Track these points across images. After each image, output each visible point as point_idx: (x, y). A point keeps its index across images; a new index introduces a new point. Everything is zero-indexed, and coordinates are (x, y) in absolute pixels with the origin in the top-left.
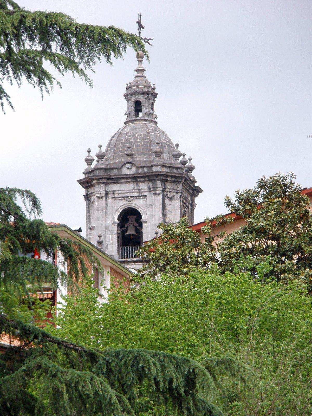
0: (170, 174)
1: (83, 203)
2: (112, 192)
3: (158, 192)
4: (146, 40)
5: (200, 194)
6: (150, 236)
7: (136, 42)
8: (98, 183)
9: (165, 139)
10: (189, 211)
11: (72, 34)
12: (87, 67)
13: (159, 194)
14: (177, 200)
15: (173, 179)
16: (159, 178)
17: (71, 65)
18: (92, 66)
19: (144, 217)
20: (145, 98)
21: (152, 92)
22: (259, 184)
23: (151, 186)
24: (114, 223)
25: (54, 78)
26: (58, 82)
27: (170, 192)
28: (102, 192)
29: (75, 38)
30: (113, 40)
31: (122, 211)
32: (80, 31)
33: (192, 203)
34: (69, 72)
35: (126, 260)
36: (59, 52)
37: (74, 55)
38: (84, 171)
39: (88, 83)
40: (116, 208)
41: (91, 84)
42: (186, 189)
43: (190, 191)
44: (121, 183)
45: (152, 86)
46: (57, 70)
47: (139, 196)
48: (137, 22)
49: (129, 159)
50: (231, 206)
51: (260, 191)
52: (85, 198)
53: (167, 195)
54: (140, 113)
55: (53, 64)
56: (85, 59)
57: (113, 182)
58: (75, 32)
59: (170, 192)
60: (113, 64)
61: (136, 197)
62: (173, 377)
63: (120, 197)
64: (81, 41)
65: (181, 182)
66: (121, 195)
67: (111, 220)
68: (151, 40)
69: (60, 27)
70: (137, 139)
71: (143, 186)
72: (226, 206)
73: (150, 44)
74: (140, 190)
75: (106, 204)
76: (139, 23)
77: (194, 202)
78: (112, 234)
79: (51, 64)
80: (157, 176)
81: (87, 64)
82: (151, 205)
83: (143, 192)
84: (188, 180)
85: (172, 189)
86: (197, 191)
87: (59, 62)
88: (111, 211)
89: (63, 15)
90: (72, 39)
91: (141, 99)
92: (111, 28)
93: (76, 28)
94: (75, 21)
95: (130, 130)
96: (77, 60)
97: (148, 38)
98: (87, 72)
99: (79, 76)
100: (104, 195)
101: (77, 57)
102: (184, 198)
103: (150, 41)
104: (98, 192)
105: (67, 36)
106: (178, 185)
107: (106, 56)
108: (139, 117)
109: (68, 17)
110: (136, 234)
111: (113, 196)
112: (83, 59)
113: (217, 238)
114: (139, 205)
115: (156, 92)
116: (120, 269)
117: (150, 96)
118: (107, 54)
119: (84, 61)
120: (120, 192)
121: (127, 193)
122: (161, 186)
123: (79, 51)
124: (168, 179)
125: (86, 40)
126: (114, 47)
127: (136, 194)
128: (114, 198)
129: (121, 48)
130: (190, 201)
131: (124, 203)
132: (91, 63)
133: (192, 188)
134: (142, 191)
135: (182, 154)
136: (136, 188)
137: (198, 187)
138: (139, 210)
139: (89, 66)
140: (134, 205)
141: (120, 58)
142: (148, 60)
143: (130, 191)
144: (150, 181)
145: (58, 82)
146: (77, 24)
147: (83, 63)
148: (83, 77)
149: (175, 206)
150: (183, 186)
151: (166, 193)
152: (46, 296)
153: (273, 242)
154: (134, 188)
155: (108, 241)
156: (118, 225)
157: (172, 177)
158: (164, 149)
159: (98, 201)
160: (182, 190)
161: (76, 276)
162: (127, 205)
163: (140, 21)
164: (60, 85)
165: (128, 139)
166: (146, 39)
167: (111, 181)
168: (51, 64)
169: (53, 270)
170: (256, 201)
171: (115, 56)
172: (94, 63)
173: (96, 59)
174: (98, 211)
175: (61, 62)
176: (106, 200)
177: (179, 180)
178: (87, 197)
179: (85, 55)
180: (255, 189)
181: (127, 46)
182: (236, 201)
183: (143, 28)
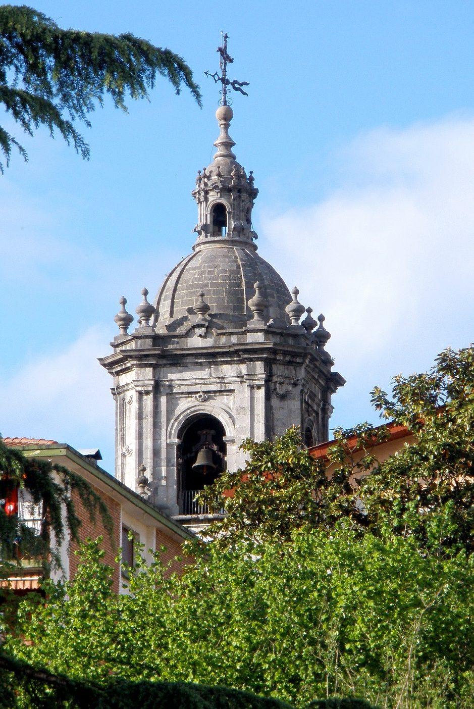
0: (281, 348)
3: (257, 382)
4: (237, 86)
5: (339, 388)
7: (176, 66)
9: (271, 280)
10: (318, 422)
11: (47, 51)
12: (76, 115)
15: (288, 358)
17: (45, 111)
18: (87, 115)
21: (248, 187)
22: (441, 363)
23: (244, 372)
25: (13, 141)
26: (21, 148)
27: (281, 383)
28: (147, 383)
29: (54, 57)
30: (130, 61)
32: (63, 42)
33: (324, 405)
34: (44, 127)
35: (194, 516)
36: (21, 86)
37: (50, 92)
38: (112, 341)
39: (79, 149)
41: (86, 153)
42: (314, 377)
43: (320, 381)
45: (248, 175)
46: (19, 123)
47: (220, 391)
48: (220, 50)
50: (384, 406)
51: (443, 376)
53: (275, 389)
54: (224, 228)
55: (11, 111)
56: (73, 100)
58: (54, 45)
59: (281, 383)
60: (129, 110)
64: (64, 64)
68: (246, 84)
69: (22, 35)
71: (229, 371)
72: (374, 407)
73: (244, 93)
76: (223, 51)
77: (329, 404)
79: (7, 111)
80: (254, 351)
81: (77, 111)
83: (228, 383)
84: (317, 360)
85: (286, 377)
86: (336, 381)
87: (24, 107)
89: (28, 12)
90: (48, 61)
92: (127, 38)
93: (56, 38)
94: (54, 24)
95: (203, 262)
96: (56, 101)
97: (240, 82)
98: (78, 125)
99: (62, 135)
101: (56, 95)
102: (309, 396)
103: (244, 88)
105: (38, 53)
106: (298, 369)
107: (114, 93)
108: (221, 235)
109: (40, 15)
110: (215, 466)
111: (168, 391)
112: (68, 99)
113: (359, 470)
114: (216, 408)
115: (255, 187)
116: (176, 532)
117: (244, 196)
118: (117, 90)
119: (71, 104)
120: (184, 382)
122: (263, 372)
123: (62, 84)
125: (76, 62)
126: (131, 77)
127: (214, 388)
129: (145, 79)
130: (320, 401)
131: (191, 404)
132: (85, 109)
133: (325, 376)
134: (226, 380)
135: (306, 308)
136: (214, 375)
137: (336, 374)
139: (79, 114)
141: (143, 97)
142: (199, 102)
143: (203, 381)
145: (21, 148)
146: (57, 29)
147: (69, 107)
148: (70, 137)
150: (307, 372)
151: (272, 386)
152: (27, 586)
153: (468, 478)
154: (211, 375)
157: (285, 353)
158: (270, 299)
160: (304, 379)
161: (57, 535)
163: (226, 47)
164: (25, 155)
166: (235, 82)
167: (165, 362)
168: (7, 111)
169: (5, 521)
170: (434, 397)
171: (133, 94)
172: (91, 108)
173: (95, 101)
175: (28, 107)
177: (298, 357)
179: (73, 93)
180: (431, 372)
181: (157, 73)
182: (394, 397)
183: (231, 61)
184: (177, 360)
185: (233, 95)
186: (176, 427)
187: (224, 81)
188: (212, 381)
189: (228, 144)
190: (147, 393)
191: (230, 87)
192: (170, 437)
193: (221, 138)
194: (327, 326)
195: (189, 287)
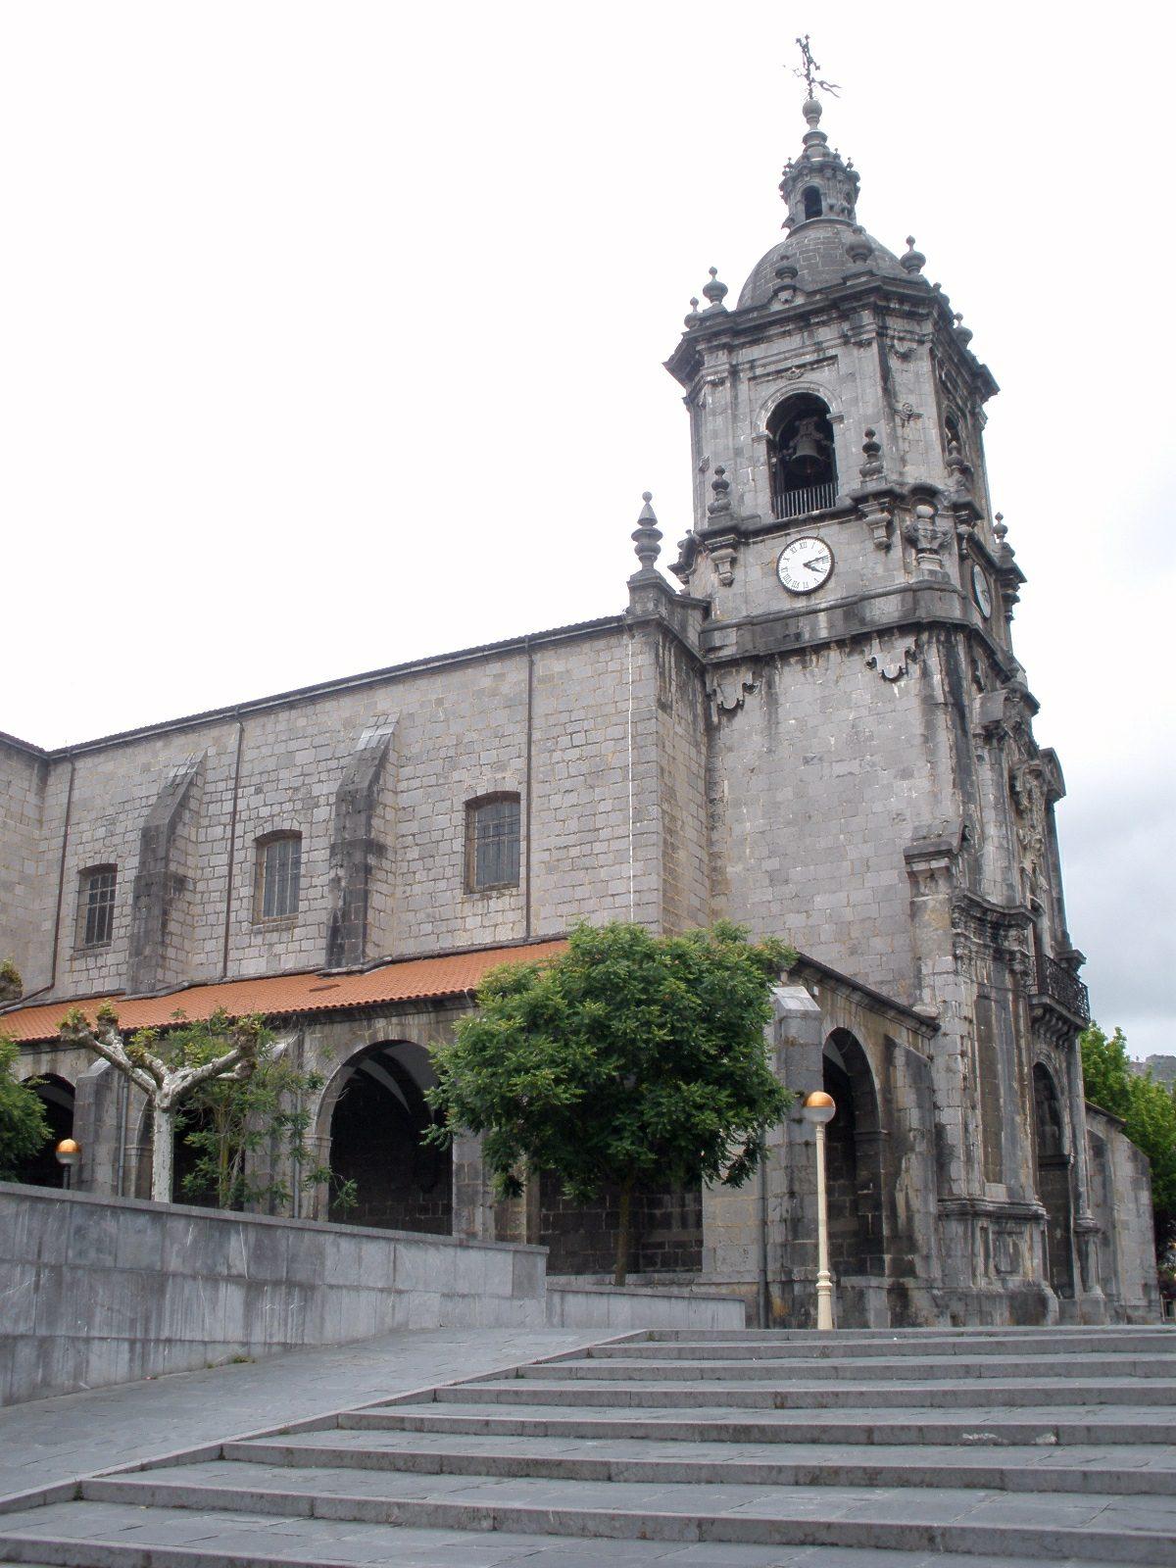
1: (684, 417)
2: (747, 366)
3: (865, 337)
6: (854, 450)
8: (709, 348)
13: (869, 343)
14: (921, 359)
15: (906, 308)
16: (866, 301)
20: (828, 179)
24: (757, 439)
31: (777, 407)
40: (760, 402)
44: (769, 339)
49: (787, 281)
52: (686, 403)
53: (893, 346)
57: (746, 340)
59: (901, 339)
63: (768, 374)
65: (928, 315)
66: (772, 368)
67: (748, 431)
71: (827, 334)
74: (819, 343)
75: (736, 397)
78: (755, 467)
82: (852, 375)
88: (747, 410)
91: (816, 181)
100: (726, 374)
104: (710, 371)
111: (751, 375)
114: (821, 382)
120: (767, 360)
121: (786, 359)
127: (808, 358)
128: (754, 378)
131: (782, 385)
134: (825, 345)
138: (821, 395)
140: (806, 385)
144: (844, 317)
149: (917, 375)
155: (745, 484)
156: (769, 442)
159: (713, 393)
162: (789, 388)
174: (714, 415)
176: (734, 386)
178: (692, 402)
188: (805, 350)
189: (812, 112)
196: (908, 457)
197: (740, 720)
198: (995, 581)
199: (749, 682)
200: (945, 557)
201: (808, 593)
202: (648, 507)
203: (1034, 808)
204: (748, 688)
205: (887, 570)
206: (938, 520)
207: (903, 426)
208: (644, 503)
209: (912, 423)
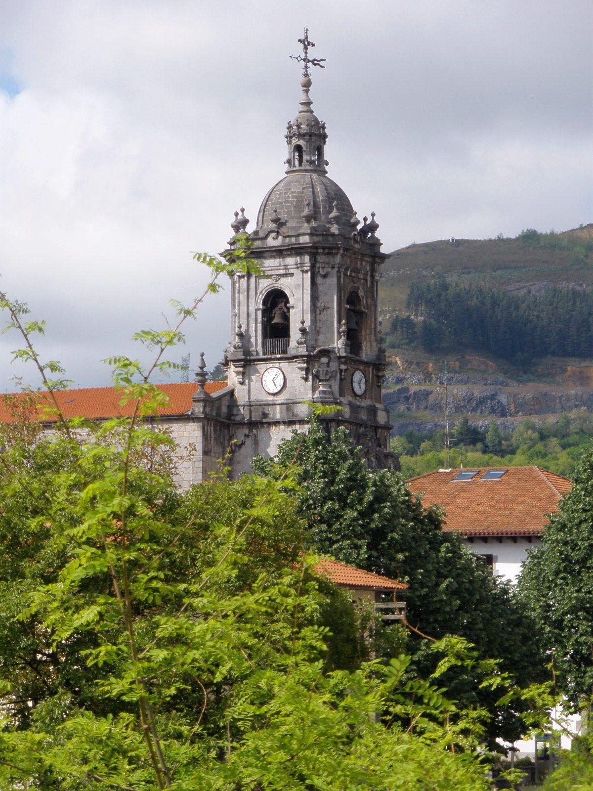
3: (305, 268)
4: (316, 62)
14: (332, 277)
15: (326, 251)
19: (292, 301)
59: (323, 268)
61: (284, 275)
62: (545, 461)
70: (289, 197)
71: (291, 261)
73: (322, 67)
74: (286, 265)
97: (319, 59)
103: (321, 63)
114: (286, 285)
122: (308, 261)
124: (319, 251)
127: (282, 272)
131: (269, 283)
134: (289, 267)
151: (316, 270)
157: (324, 248)
163: (307, 37)
165: (279, 198)
184: (260, 254)
185: (312, 68)
186: (261, 298)
187: (305, 60)
189: (308, 103)
190: (243, 277)
191: (310, 64)
192: (257, 304)
193: (302, 98)
194: (377, 220)
195: (273, 204)
196: (322, 330)
197: (243, 450)
198: (373, 369)
199: (247, 433)
200: (333, 382)
201: (274, 394)
202: (203, 360)
203: (488, 387)
204: (247, 436)
205: (305, 389)
206: (331, 364)
207: (320, 314)
208: (235, 217)
209: (325, 311)
